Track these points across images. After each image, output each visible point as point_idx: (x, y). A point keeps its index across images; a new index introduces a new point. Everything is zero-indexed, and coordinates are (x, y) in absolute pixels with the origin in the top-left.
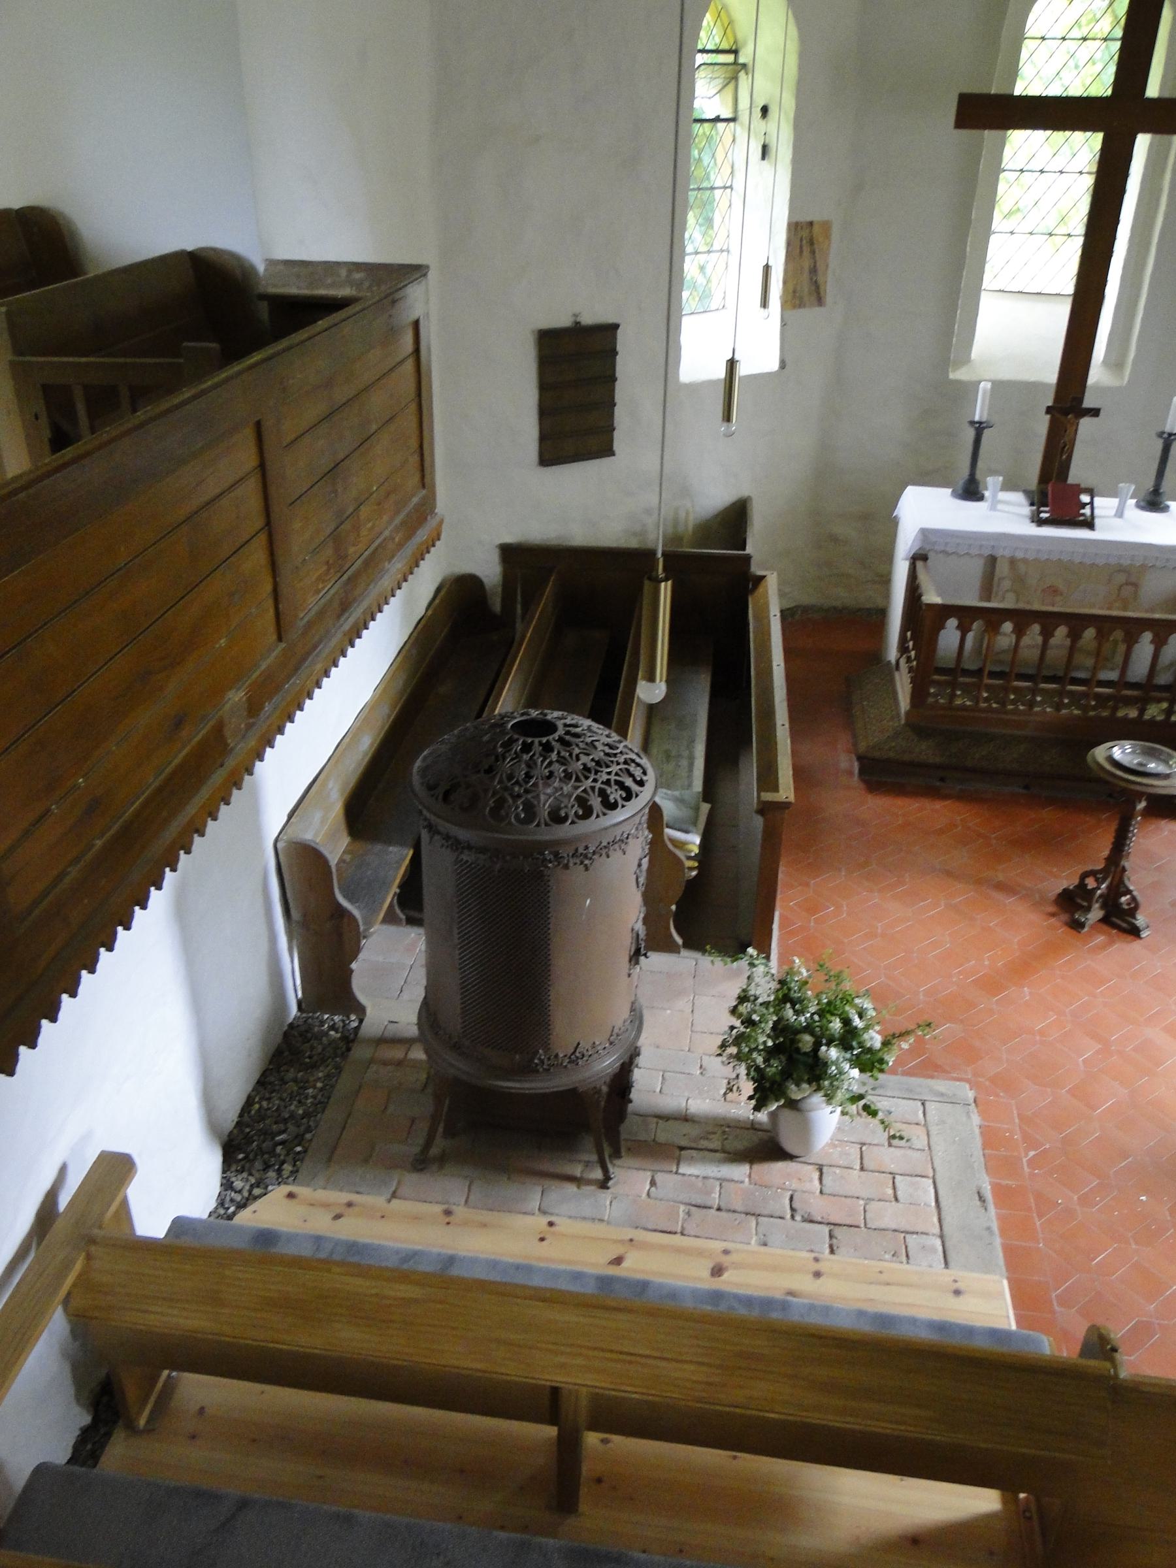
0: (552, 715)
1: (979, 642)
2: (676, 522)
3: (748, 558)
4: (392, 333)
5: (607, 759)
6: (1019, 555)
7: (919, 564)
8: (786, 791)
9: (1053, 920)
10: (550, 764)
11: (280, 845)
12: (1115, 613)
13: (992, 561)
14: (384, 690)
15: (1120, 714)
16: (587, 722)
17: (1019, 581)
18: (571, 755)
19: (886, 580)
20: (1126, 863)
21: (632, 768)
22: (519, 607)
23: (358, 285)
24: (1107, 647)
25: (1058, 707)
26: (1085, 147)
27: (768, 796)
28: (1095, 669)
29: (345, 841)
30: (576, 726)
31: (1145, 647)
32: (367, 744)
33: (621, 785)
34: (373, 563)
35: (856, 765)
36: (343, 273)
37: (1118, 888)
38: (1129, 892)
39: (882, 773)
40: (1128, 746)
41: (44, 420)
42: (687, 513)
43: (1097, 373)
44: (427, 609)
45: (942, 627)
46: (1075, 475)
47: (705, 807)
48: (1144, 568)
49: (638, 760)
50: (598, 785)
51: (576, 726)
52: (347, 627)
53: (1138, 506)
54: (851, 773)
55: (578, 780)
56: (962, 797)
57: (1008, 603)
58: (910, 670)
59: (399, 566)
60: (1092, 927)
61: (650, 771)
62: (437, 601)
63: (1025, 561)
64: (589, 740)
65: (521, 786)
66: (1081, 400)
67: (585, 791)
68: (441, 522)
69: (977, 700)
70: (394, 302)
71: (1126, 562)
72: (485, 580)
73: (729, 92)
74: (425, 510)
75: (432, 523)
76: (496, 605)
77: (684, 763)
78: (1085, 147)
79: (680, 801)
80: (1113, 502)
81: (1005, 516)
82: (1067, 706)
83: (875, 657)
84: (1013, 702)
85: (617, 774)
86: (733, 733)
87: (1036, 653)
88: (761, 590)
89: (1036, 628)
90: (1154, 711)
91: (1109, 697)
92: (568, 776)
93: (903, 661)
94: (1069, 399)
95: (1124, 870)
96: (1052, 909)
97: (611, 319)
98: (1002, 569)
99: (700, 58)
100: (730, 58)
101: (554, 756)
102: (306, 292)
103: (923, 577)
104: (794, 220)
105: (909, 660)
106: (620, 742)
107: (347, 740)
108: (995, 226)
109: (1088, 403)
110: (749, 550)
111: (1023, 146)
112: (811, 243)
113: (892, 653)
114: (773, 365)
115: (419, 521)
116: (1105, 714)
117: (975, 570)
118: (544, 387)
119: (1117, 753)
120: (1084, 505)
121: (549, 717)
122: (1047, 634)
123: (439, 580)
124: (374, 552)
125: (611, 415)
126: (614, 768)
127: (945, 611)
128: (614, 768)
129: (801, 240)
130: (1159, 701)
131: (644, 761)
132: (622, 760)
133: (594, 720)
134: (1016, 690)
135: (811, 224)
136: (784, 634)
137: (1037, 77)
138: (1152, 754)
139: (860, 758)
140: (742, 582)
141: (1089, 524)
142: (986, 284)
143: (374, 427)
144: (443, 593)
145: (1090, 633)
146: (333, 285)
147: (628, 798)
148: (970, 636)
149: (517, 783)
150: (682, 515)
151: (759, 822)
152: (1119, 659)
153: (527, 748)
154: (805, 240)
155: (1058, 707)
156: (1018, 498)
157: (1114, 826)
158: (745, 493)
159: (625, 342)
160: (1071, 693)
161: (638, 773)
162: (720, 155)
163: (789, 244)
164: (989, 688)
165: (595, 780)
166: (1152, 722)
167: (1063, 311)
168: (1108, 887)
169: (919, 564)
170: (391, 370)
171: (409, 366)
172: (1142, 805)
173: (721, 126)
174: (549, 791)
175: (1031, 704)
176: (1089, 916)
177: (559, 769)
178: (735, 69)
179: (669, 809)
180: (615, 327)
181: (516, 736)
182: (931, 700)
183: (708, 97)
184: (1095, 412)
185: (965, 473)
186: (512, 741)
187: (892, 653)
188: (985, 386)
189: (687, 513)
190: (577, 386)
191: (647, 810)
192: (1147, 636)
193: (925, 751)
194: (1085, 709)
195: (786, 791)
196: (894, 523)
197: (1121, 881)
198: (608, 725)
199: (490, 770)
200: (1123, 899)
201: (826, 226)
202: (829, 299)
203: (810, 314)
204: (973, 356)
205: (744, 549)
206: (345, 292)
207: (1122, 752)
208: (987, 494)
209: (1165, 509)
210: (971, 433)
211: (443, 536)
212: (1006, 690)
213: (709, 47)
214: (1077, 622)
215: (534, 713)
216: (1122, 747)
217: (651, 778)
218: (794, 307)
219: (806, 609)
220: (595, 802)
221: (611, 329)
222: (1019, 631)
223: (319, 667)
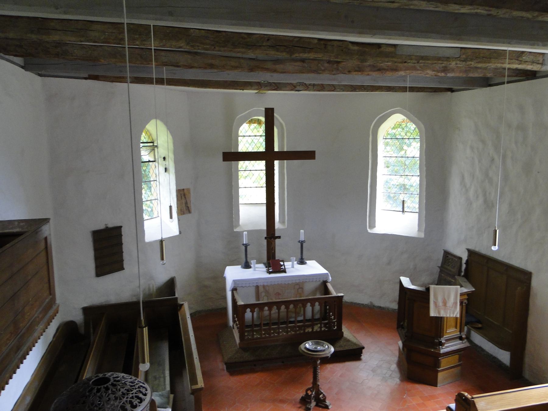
0: (108, 374)
1: (258, 314)
2: (149, 289)
3: (176, 299)
5: (131, 388)
6: (265, 284)
7: (234, 292)
8: (201, 383)
9: (300, 409)
12: (298, 299)
13: (257, 287)
14: (36, 376)
15: (306, 331)
16: (123, 374)
17: (267, 292)
18: (117, 390)
19: (225, 298)
20: (319, 383)
21: (141, 389)
25: (287, 332)
26: (261, 165)
27: (195, 387)
28: (296, 318)
30: (118, 377)
31: (309, 307)
32: (28, 399)
33: (138, 397)
34: (30, 329)
35: (225, 366)
36: (16, 223)
37: (318, 393)
38: (322, 393)
39: (234, 368)
40: (310, 342)
42: (153, 286)
43: (278, 225)
45: (245, 312)
46: (278, 256)
47: (172, 396)
48: (303, 283)
49: (143, 385)
50: (129, 399)
51: (118, 377)
52: (19, 356)
53: (298, 264)
54: (224, 370)
55: (120, 399)
56: (263, 370)
57: (265, 301)
58: (238, 328)
59: (41, 327)
60: (313, 409)
61: (149, 389)
62: (57, 334)
63: (267, 286)
64: (123, 382)
66: (274, 234)
67: (124, 403)
68: (59, 306)
69: (261, 335)
70: (37, 233)
71: (298, 282)
72: (77, 322)
73: (152, 154)
75: (55, 307)
76: (82, 331)
77: (162, 379)
78: (261, 165)
79: (161, 396)
80: (290, 263)
81: (258, 272)
82: (290, 332)
83: (225, 325)
84: (273, 333)
85: (136, 393)
86: (179, 364)
87: (277, 315)
88: (182, 309)
89: (275, 307)
90: (316, 328)
91: (302, 326)
92: (116, 398)
93: (235, 325)
94: (271, 234)
95: (319, 386)
96: (299, 405)
97: (119, 225)
98: (261, 289)
99: (142, 145)
100: (151, 144)
101: (110, 392)
103: (236, 296)
105: (237, 325)
106: (136, 380)
107: (19, 400)
109: (277, 235)
110: (177, 296)
111: (242, 164)
112: (184, 195)
113: (231, 323)
114: (176, 232)
115: (49, 306)
116: (302, 332)
117: (253, 291)
118: (96, 250)
119: (307, 346)
120: (282, 266)
121: (107, 376)
122: (279, 309)
125: (122, 256)
126: (135, 391)
127: (246, 306)
128: (135, 391)
130: (317, 324)
131: (146, 385)
132: (137, 387)
133: (125, 373)
134: (273, 329)
136: (193, 325)
137: (244, 146)
138: (317, 344)
139: (226, 364)
140: (176, 307)
141: (284, 271)
142: (241, 201)
143: (30, 277)
144: (60, 330)
145: (291, 306)
146: (12, 228)
147: (141, 402)
148: (255, 314)
150: (151, 286)
151: (192, 397)
153: (99, 390)
154: (182, 195)
155: (287, 332)
156: (262, 265)
157: (312, 370)
158: (172, 275)
159: (124, 231)
160: (290, 327)
161: (143, 390)
162: (151, 171)
163: (177, 196)
164: (264, 330)
165: (127, 398)
167: (264, 209)
169: (234, 292)
171: (43, 254)
172: (319, 362)
174: (109, 406)
175: (279, 333)
176: (312, 405)
177: (112, 396)
178: (153, 146)
179: (158, 400)
182: (246, 338)
183: (145, 155)
184: (279, 237)
185: (244, 260)
186: (92, 389)
187: (231, 323)
188: (245, 233)
189: (153, 286)
190: (109, 249)
191: (149, 405)
192: (309, 304)
193: (247, 356)
194: (296, 331)
195: (201, 383)
196: (224, 279)
197: (319, 390)
198: (130, 374)
199: (84, 402)
200: (321, 396)
201: (188, 190)
203: (187, 216)
204: (240, 223)
206: (17, 230)
207: (308, 345)
208: (252, 266)
209: (305, 263)
210: (244, 248)
211: (59, 312)
212: (270, 329)
213: (145, 141)
214: (287, 303)
215: (101, 375)
216: (308, 343)
217: (149, 391)
218: (181, 214)
219: (199, 312)
221: (121, 227)
222: (270, 309)
223: (8, 375)
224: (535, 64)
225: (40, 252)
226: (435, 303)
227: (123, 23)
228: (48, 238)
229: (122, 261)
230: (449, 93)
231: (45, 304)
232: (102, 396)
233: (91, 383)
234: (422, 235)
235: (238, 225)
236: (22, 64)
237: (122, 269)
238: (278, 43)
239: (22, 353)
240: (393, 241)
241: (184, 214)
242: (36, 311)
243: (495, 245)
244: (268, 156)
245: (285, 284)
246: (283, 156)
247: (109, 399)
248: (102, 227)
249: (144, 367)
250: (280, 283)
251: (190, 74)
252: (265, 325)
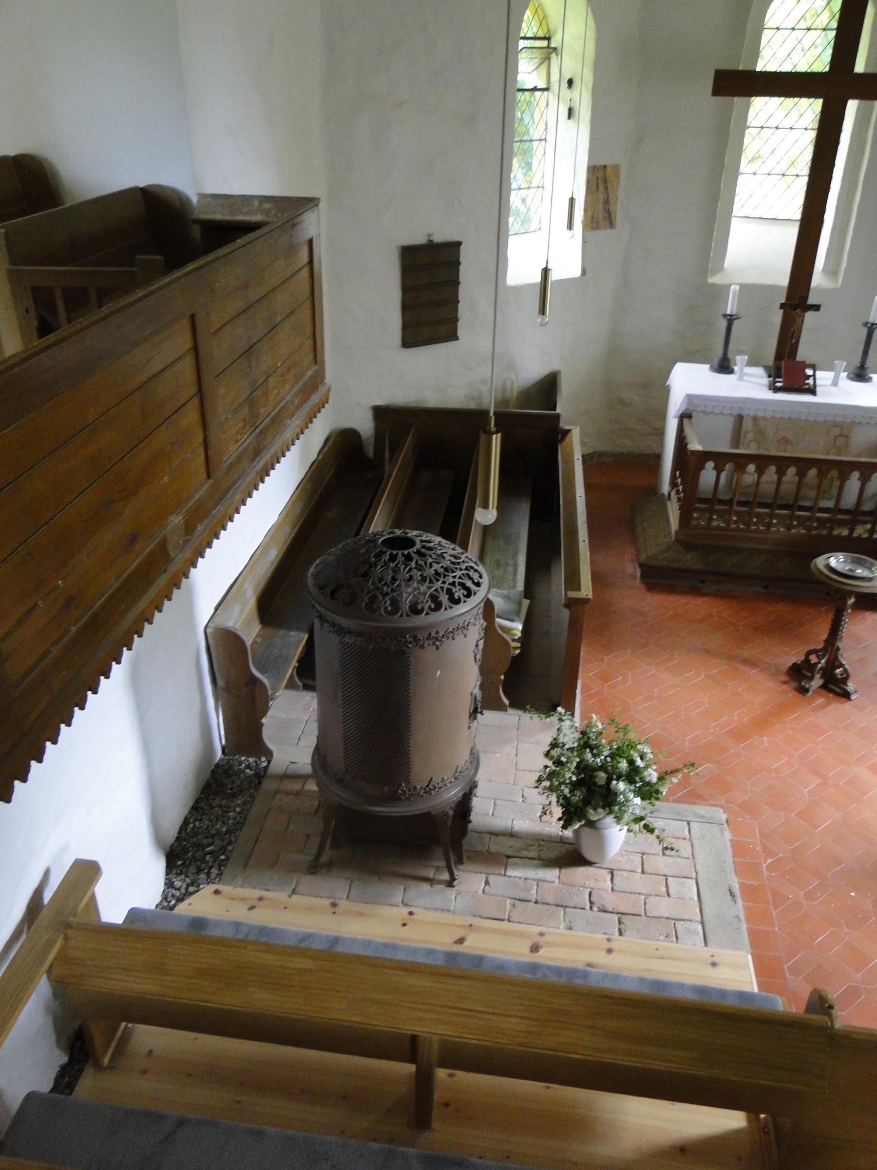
0: (412, 534)
1: (730, 479)
2: (504, 390)
3: (558, 417)
4: (292, 248)
5: (453, 566)
6: (760, 414)
7: (686, 421)
8: (586, 590)
9: (785, 687)
10: (410, 570)
11: (208, 631)
12: (831, 457)
13: (740, 418)
14: (287, 515)
16: (438, 539)
17: (760, 433)
18: (426, 563)
19: (660, 433)
21: (471, 573)
22: (387, 453)
23: (267, 212)
24: (825, 482)
25: (789, 527)
27: (573, 594)
28: (817, 499)
29: (257, 627)
30: (429, 542)
31: (854, 483)
32: (274, 555)
33: (463, 586)
34: (278, 421)
35: (638, 571)
36: (256, 203)
37: (834, 663)
38: (842, 665)
39: (658, 577)
40: (841, 557)
41: (33, 314)
42: (513, 383)
43: (818, 278)
44: (318, 455)
45: (703, 468)
46: (802, 355)
47: (526, 602)
48: (853, 424)
49: (476, 567)
50: (446, 586)
51: (429, 542)
53: (849, 377)
54: (634, 577)
55: (431, 582)
57: (752, 450)
58: (679, 500)
59: (297, 422)
60: (815, 692)
61: (485, 575)
62: (326, 449)
63: (764, 418)
64: (439, 552)
65: (388, 586)
66: (806, 298)
67: (436, 590)
68: (329, 389)
69: (728, 522)
70: (294, 225)
71: (839, 419)
72: (362, 433)
74: (317, 381)
75: (322, 390)
76: (370, 451)
77: (510, 569)
78: (809, 110)
79: (507, 598)
80: (830, 375)
81: (749, 385)
83: (653, 490)
85: (460, 578)
86: (547, 547)
87: (773, 487)
88: (567, 440)
89: (773, 468)
90: (861, 531)
91: (827, 520)
92: (423, 579)
93: (673, 493)
94: (797, 298)
95: (838, 649)
96: (785, 678)
97: (455, 238)
98: (748, 425)
99: (522, 44)
100: (544, 43)
101: (413, 564)
102: (228, 218)
104: (592, 164)
105: (678, 492)
106: (463, 553)
107: (259, 552)
108: (742, 168)
109: (811, 300)
110: (558, 410)
111: (763, 109)
112: (605, 181)
113: (666, 488)
114: (577, 272)
115: (312, 389)
116: (824, 533)
117: (727, 425)
119: (833, 562)
120: (808, 377)
121: (409, 535)
122: (781, 473)
125: (456, 310)
126: (458, 573)
127: (705, 456)
128: (458, 573)
129: (598, 179)
130: (865, 523)
131: (480, 568)
132: (464, 567)
133: (443, 537)
134: (758, 515)
135: (605, 167)
137: (773, 57)
138: (859, 563)
139: (641, 566)
140: (553, 434)
141: (812, 391)
142: (735, 212)
143: (279, 319)
144: (330, 442)
145: (813, 472)
146: (248, 213)
147: (468, 596)
148: (723, 475)
149: (386, 584)
150: (509, 384)
151: (566, 613)
152: (834, 492)
153: (393, 558)
154: (600, 179)
155: (789, 527)
156: (759, 371)
157: (831, 616)
158: (555, 367)
159: (466, 255)
160: (799, 517)
161: (475, 577)
162: (537, 115)
163: (588, 182)
164: (737, 513)
165: (444, 582)
166: (859, 539)
167: (793, 233)
168: (826, 662)
169: (686, 421)
170: (292, 276)
171: (305, 273)
172: (851, 601)
173: (538, 94)
174: (409, 590)
175: (769, 525)
176: (812, 684)
177: (417, 574)
178: (548, 52)
179: (499, 603)
180: (458, 244)
181: (385, 549)
182: (694, 522)
183: (528, 73)
184: (817, 308)
185: (719, 353)
186: (382, 553)
187: (666, 488)
188: (735, 288)
190: (430, 288)
191: (482, 605)
192: (856, 475)
193: (690, 560)
194: (809, 529)
195: (586, 590)
196: (667, 390)
197: (836, 658)
198: (453, 541)
199: (365, 575)
200: (838, 671)
201: (616, 169)
202: (618, 223)
203: (604, 234)
204: (726, 265)
205: (555, 410)
206: (257, 218)
207: (837, 561)
208: (736, 368)
209: (869, 380)
210: (724, 323)
211: (330, 400)
212: (750, 515)
213: (529, 35)
214: (803, 464)
215: (398, 532)
216: (837, 557)
217: (485, 581)
218: (592, 229)
219: (601, 455)
220: (444, 598)
221: (456, 246)
222: (760, 471)
223: (238, 497)
235: (719, 268)
239: (262, 463)
242: (290, 390)
247: (411, 577)
249: (486, 516)
252: (740, 503)
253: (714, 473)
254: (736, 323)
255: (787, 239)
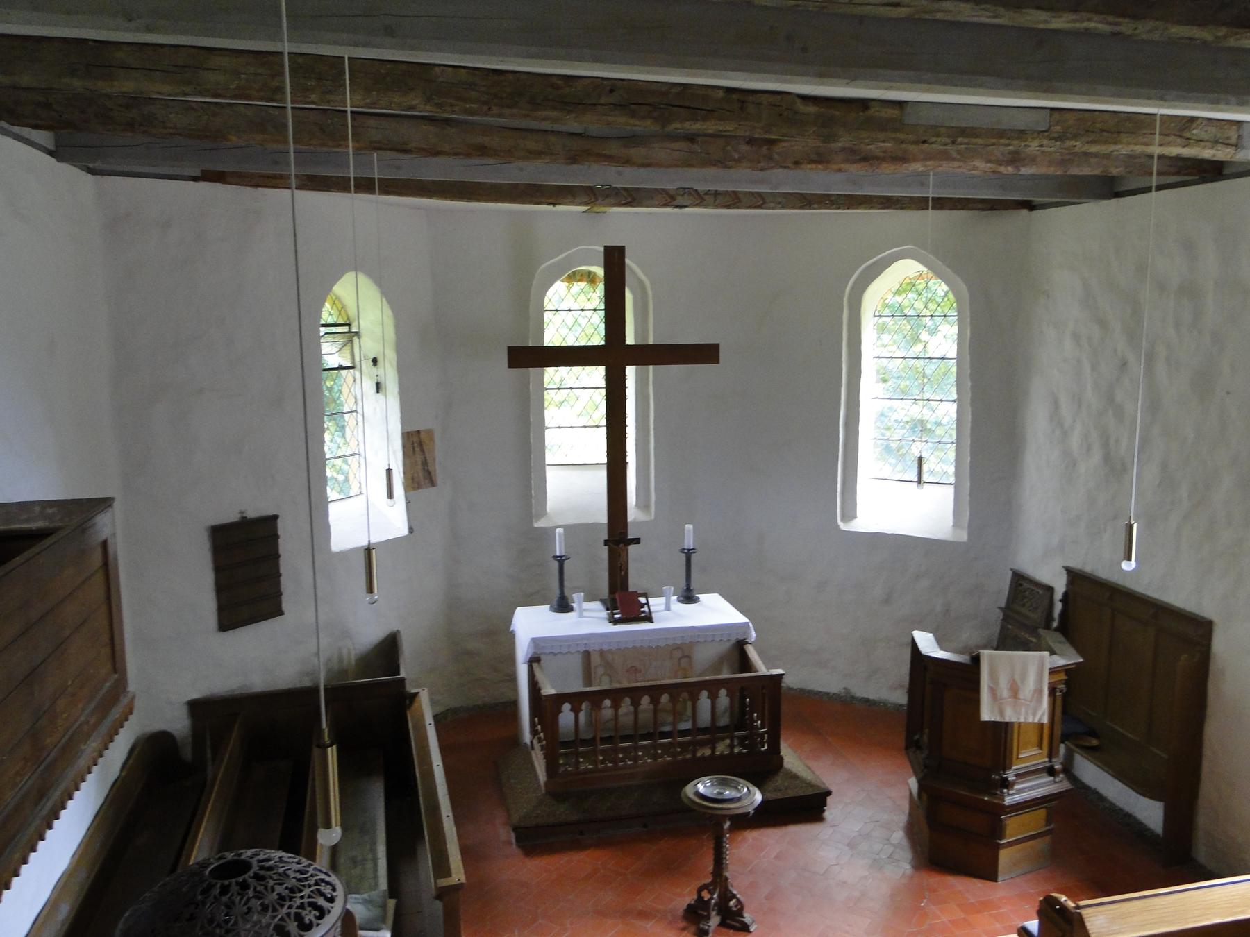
0: (247, 854)
1: (589, 715)
2: (340, 659)
3: (403, 680)
5: (298, 884)
6: (605, 648)
7: (535, 665)
8: (458, 874)
9: (685, 933)
10: (248, 900)
12: (679, 681)
13: (587, 655)
15: (699, 754)
16: (280, 854)
17: (608, 666)
18: (266, 888)
19: (513, 679)
20: (727, 874)
21: (322, 888)
22: (209, 751)
24: (679, 707)
26: (596, 375)
27: (444, 882)
28: (674, 724)
30: (268, 860)
31: (704, 701)
32: (65, 911)
33: (314, 906)
34: (69, 750)
35: (513, 835)
36: (37, 509)
37: (726, 896)
38: (734, 896)
39: (535, 839)
40: (707, 781)
42: (349, 653)
43: (633, 513)
44: (122, 769)
46: (634, 584)
47: (392, 903)
48: (692, 645)
49: (327, 879)
50: (293, 910)
51: (268, 860)
54: (510, 843)
55: (275, 910)
56: (601, 844)
57: (605, 686)
58: (542, 748)
59: (94, 745)
60: (715, 932)
61: (339, 887)
62: (131, 761)
63: (610, 651)
64: (281, 870)
67: (282, 919)
68: (134, 697)
69: (595, 763)
70: (84, 531)
71: (679, 642)
72: (178, 738)
73: (347, 351)
75: (124, 701)
76: (187, 754)
77: (369, 865)
78: (596, 375)
80: (662, 600)
81: (589, 620)
82: (661, 756)
83: (514, 740)
85: (310, 897)
86: (408, 830)
87: (632, 717)
88: (416, 705)
89: (627, 700)
91: (689, 743)
92: (265, 908)
93: (535, 742)
94: (618, 533)
95: (727, 879)
96: (682, 924)
97: (271, 513)
98: (596, 659)
99: (323, 330)
100: (345, 329)
101: (251, 893)
103: (539, 676)
105: (540, 740)
106: (310, 865)
107: (44, 913)
109: (631, 535)
110: (403, 674)
111: (553, 375)
112: (421, 444)
113: (527, 737)
114: (402, 530)
115: (113, 698)
116: (688, 756)
117: (576, 663)
118: (219, 569)
119: (701, 788)
120: (643, 605)
121: (243, 857)
122: (636, 704)
123: (132, 741)
124: (70, 739)
125: (278, 584)
126: (307, 891)
127: (560, 699)
128: (307, 891)
130: (723, 739)
131: (333, 879)
132: (312, 882)
133: (285, 851)
134: (624, 750)
137: (556, 334)
138: (724, 783)
139: (515, 829)
140: (402, 700)
141: (649, 619)
142: (549, 459)
143: (68, 632)
144: (136, 752)
145: (665, 698)
146: (27, 521)
147: (321, 917)
148: (582, 716)
150: (345, 652)
151: (439, 905)
152: (689, 712)
153: (225, 890)
154: (416, 445)
155: (655, 757)
156: (597, 605)
157: (711, 844)
158: (393, 626)
159: (283, 527)
160: (661, 744)
161: (327, 890)
162: (345, 390)
163: (404, 447)
165: (290, 907)
166: (722, 756)
167: (602, 476)
168: (719, 896)
169: (535, 665)
170: (84, 582)
171: (99, 578)
172: (727, 825)
173: (344, 372)
174: (248, 926)
175: (636, 759)
176: (711, 923)
178: (349, 334)
179: (360, 912)
180: (276, 517)
182: (562, 770)
183: (332, 354)
184: (637, 541)
186: (211, 887)
187: (527, 737)
189: (349, 653)
190: (248, 567)
191: (339, 924)
192: (704, 694)
193: (564, 812)
194: (674, 755)
195: (458, 874)
196: (511, 636)
197: (727, 889)
198: (297, 853)
200: (732, 903)
201: (430, 433)
203: (427, 493)
204: (548, 510)
206: (39, 524)
207: (704, 786)
208: (575, 605)
209: (696, 601)
210: (556, 564)
211: (135, 711)
212: (616, 750)
213: (330, 321)
214: (654, 692)
215: (230, 856)
216: (704, 783)
217: (340, 893)
218: (414, 489)
219: (454, 711)
222: (616, 705)
223: (17, 856)
224: (1219, 147)
225: (92, 575)
226: (993, 691)
227: (282, 53)
228: (110, 542)
229: (278, 594)
230: (1025, 212)
231: (101, 693)
232: (233, 903)
233: (207, 872)
234: (963, 536)
235: (543, 512)
236: (52, 147)
237: (279, 612)
238: (635, 99)
239: (49, 804)
240: (896, 549)
241: (419, 487)
242: (83, 710)
243: (1129, 559)
244: (612, 355)
245: (650, 647)
246: (646, 355)
247: (249, 909)
248: (233, 517)
249: (329, 837)
250: (638, 645)
251: (433, 169)
253: (572, 715)
254: (566, 564)
255: (600, 479)
